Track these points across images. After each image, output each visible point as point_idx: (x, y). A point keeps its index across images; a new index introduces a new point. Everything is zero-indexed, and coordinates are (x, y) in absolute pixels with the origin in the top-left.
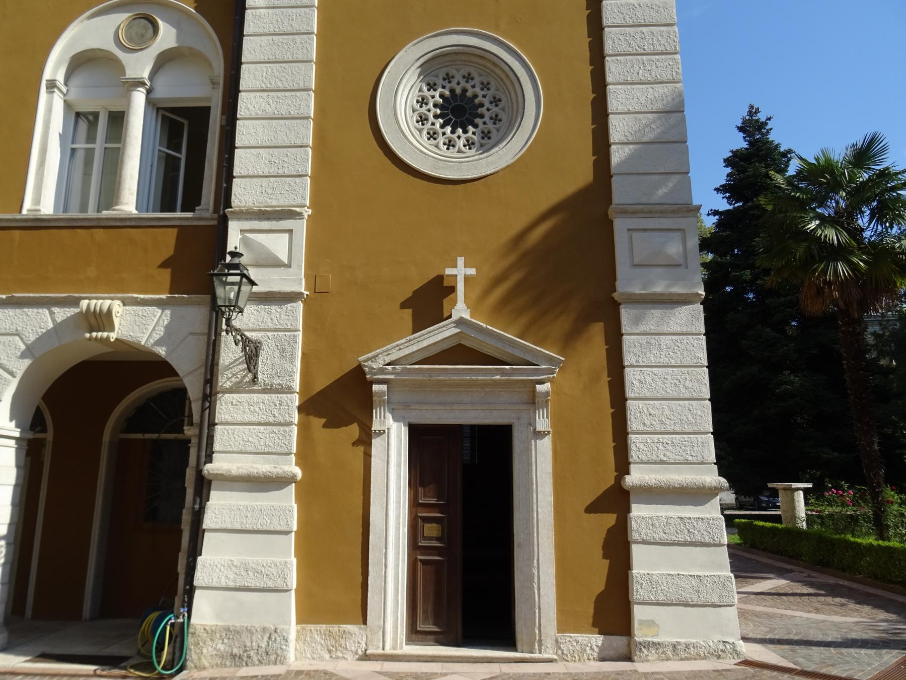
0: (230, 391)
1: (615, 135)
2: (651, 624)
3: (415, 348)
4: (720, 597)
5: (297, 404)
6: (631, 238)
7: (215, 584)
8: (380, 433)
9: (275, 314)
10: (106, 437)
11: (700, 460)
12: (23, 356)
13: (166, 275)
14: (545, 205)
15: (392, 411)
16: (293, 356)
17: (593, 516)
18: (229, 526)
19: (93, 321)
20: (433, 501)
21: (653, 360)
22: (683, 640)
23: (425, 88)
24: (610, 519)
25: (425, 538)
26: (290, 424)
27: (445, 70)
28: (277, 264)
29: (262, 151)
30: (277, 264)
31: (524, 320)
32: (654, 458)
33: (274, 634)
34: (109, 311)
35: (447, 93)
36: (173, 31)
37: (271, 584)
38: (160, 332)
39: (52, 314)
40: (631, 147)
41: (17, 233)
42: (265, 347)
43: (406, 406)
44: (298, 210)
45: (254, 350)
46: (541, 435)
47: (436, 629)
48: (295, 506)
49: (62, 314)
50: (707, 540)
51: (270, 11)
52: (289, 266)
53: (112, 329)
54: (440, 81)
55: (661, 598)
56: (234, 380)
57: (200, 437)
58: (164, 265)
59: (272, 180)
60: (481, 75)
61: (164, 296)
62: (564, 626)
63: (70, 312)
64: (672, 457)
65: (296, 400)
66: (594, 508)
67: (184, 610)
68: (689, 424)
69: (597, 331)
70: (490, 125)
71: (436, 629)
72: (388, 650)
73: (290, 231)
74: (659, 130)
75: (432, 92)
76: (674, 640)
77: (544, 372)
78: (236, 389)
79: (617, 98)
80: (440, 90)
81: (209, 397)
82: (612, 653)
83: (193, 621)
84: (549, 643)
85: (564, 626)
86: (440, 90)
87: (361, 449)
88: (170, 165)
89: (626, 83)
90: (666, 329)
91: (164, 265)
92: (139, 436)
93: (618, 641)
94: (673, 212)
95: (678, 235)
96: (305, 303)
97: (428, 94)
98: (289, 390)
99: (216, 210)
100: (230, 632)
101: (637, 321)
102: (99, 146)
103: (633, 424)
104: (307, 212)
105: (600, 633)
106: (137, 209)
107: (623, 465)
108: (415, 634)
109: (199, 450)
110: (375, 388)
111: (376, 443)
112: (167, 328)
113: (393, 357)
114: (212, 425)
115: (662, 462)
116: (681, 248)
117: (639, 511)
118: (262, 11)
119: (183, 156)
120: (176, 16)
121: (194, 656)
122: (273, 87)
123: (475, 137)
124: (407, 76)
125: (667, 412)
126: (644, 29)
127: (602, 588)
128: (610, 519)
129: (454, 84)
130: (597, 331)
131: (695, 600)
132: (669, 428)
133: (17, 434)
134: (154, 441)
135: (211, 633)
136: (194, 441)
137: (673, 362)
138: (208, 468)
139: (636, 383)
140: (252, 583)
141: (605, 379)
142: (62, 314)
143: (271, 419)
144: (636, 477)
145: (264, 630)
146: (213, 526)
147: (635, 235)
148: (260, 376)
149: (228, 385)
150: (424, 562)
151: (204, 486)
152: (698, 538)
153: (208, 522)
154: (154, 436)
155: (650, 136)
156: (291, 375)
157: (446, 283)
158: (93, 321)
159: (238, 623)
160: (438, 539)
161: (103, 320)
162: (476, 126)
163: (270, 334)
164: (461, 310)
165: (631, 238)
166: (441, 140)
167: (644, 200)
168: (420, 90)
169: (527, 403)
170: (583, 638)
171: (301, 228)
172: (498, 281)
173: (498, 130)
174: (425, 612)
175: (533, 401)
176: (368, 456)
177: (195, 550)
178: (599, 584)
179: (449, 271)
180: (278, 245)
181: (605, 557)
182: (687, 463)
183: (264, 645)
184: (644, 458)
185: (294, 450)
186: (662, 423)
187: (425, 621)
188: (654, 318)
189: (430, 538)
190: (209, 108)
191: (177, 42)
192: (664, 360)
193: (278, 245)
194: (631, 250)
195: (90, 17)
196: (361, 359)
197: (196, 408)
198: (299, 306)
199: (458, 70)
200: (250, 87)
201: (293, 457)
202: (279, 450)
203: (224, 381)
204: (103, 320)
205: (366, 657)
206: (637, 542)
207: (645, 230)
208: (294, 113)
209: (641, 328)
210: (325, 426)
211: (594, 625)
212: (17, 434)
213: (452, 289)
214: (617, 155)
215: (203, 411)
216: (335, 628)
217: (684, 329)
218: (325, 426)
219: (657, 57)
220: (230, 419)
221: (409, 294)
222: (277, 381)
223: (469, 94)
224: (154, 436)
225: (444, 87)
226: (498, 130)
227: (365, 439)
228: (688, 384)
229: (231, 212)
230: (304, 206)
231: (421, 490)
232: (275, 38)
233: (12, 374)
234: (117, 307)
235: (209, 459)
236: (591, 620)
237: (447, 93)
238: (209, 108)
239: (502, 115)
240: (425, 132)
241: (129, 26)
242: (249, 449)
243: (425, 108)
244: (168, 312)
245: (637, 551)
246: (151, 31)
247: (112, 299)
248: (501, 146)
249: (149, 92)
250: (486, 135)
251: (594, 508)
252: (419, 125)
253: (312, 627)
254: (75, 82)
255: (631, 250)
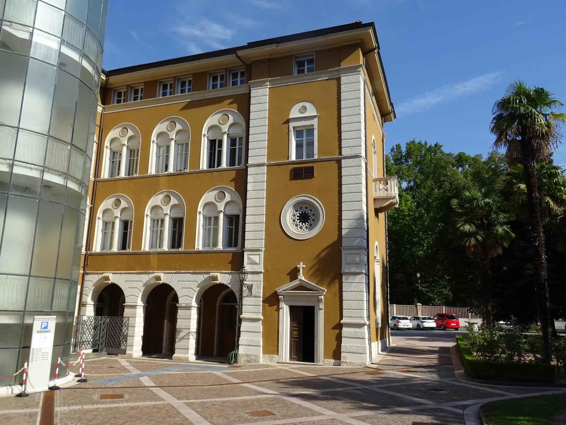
0: (246, 297)
1: (344, 226)
2: (345, 357)
3: (289, 287)
4: (363, 351)
5: (262, 300)
6: (346, 256)
7: (243, 344)
8: (282, 308)
9: (256, 277)
10: (217, 304)
11: (361, 316)
12: (198, 287)
13: (230, 265)
14: (324, 246)
15: (284, 302)
16: (260, 288)
17: (333, 330)
18: (246, 330)
19: (213, 278)
20: (296, 325)
21: (350, 290)
22: (352, 361)
23: (295, 212)
24: (338, 331)
25: (294, 335)
26: (260, 305)
27: (300, 206)
28: (256, 264)
29: (252, 232)
30: (256, 264)
31: (318, 278)
32: (349, 316)
33: (257, 356)
34: (217, 276)
35: (301, 213)
36: (229, 196)
37: (256, 344)
38: (229, 281)
39: (204, 276)
40: (348, 230)
41: (194, 255)
42: (254, 286)
43: (288, 301)
44: (261, 249)
45: (251, 287)
46: (321, 309)
47: (296, 357)
48: (262, 326)
49: (206, 276)
50: (361, 337)
51: (253, 191)
52: (259, 264)
53: (218, 280)
54: (299, 209)
55: (348, 351)
56: (247, 294)
57: (239, 308)
58: (229, 263)
59: (255, 240)
60: (310, 207)
61: (229, 272)
62: (325, 357)
63: (208, 276)
64: (354, 316)
65: (261, 299)
66: (334, 328)
67: (237, 350)
68: (359, 307)
69: (337, 281)
70: (312, 222)
71: (296, 357)
72: (284, 361)
73: (259, 255)
74: (356, 225)
75: (297, 213)
76: (350, 361)
77: (320, 293)
78: (247, 296)
79: (345, 215)
80: (299, 212)
81: (241, 298)
82: (336, 364)
83: (239, 352)
84: (321, 361)
85: (325, 357)
86: (299, 212)
87: (277, 312)
88: (230, 231)
89: (347, 211)
90: (354, 282)
91: (229, 263)
92: (226, 304)
93: (338, 361)
94: (357, 249)
95: (359, 255)
96: (263, 274)
97: (294, 218)
98: (260, 297)
99: (241, 248)
100: (247, 355)
101: (347, 279)
102: (212, 227)
103: (344, 307)
104: (264, 249)
105: (334, 359)
106: (226, 165)
107: (341, 318)
108: (291, 358)
109: (239, 312)
110: (280, 297)
111: (280, 310)
112: (231, 280)
113: (284, 289)
114: (242, 305)
115: (351, 317)
116: (359, 259)
117: (344, 330)
118: (251, 191)
119: (234, 227)
120: (230, 192)
121: (239, 360)
122: (254, 214)
123: (308, 226)
124: (289, 209)
125: (353, 304)
126: (353, 194)
127: (335, 348)
128: (338, 331)
129: (302, 210)
130: (337, 281)
131: (356, 352)
132: (353, 308)
133: (197, 306)
134: (231, 306)
135: (243, 355)
136: (238, 309)
137: (355, 290)
138: (241, 316)
139: (345, 296)
140: (252, 344)
141: (338, 295)
142: (206, 276)
143: (256, 304)
144: (344, 321)
145: (255, 355)
146: (243, 330)
147: (347, 255)
148: (253, 293)
149: (245, 295)
150: (293, 341)
151: (240, 320)
152: (359, 337)
153: (241, 329)
154: (231, 304)
155: (353, 227)
156: (260, 293)
157: (298, 269)
158: (213, 278)
159: (249, 353)
160: (297, 335)
161: (215, 278)
162: (308, 222)
163: (255, 282)
164: (301, 277)
165: (346, 256)
166: (299, 227)
167: (350, 245)
168: (293, 212)
169: (317, 301)
170: (329, 360)
171: (262, 254)
172: (312, 268)
173: (314, 224)
174: (294, 353)
175: (320, 301)
176: (279, 314)
177: (239, 336)
178: (334, 348)
179: (298, 266)
180: (256, 258)
181: (336, 340)
182: (357, 317)
183: (255, 358)
184: (346, 316)
185: (261, 312)
186: (352, 307)
187: (294, 356)
188: (351, 278)
189: (295, 335)
190: (239, 215)
191: (231, 199)
192: (353, 290)
193: (256, 258)
194: (346, 259)
195: (208, 192)
196: (276, 289)
197: (238, 301)
198: (262, 274)
199: (304, 206)
200: (249, 214)
201: (261, 314)
202: (257, 312)
203: (244, 294)
204: (215, 278)
205: (278, 363)
206: (343, 337)
207: (350, 254)
208: (260, 222)
209: (348, 281)
210: (268, 306)
211: (333, 357)
212: (197, 306)
213: (299, 270)
214: (344, 232)
215: (240, 302)
216: (271, 356)
217: (359, 282)
218: (268, 306)
219: (356, 202)
220: (246, 304)
221: (289, 272)
222: (257, 294)
223: (307, 213)
224: (231, 304)
225: (300, 211)
226: (314, 224)
227: (278, 309)
228: (359, 296)
229: (245, 250)
230: (262, 248)
231: (293, 323)
232: (255, 199)
233: (195, 292)
234: (219, 275)
235: (241, 314)
236: (332, 356)
237: (301, 213)
238: (239, 215)
239: (315, 219)
240: (294, 225)
241: (218, 195)
242: (251, 312)
243: (295, 217)
244: (231, 276)
245: (343, 340)
246: (224, 196)
247: (218, 273)
248: (313, 229)
249: (228, 135)
250: (311, 225)
251: (334, 328)
252: (293, 223)
253: (266, 355)
254: (205, 210)
255: (346, 259)
